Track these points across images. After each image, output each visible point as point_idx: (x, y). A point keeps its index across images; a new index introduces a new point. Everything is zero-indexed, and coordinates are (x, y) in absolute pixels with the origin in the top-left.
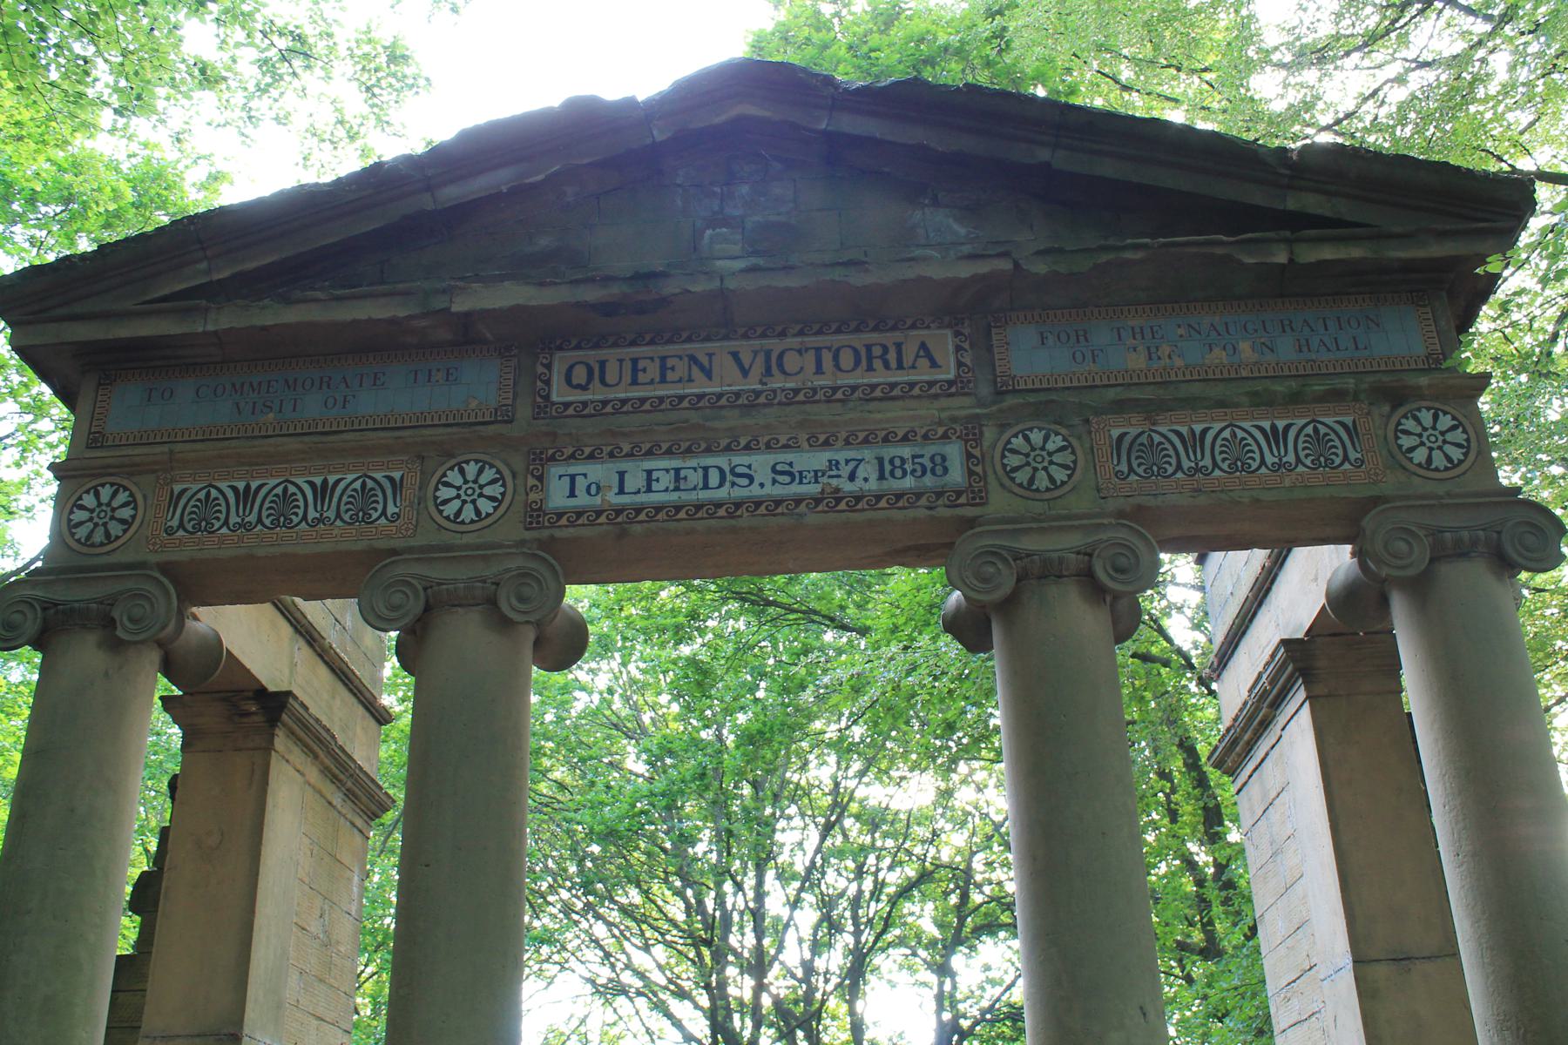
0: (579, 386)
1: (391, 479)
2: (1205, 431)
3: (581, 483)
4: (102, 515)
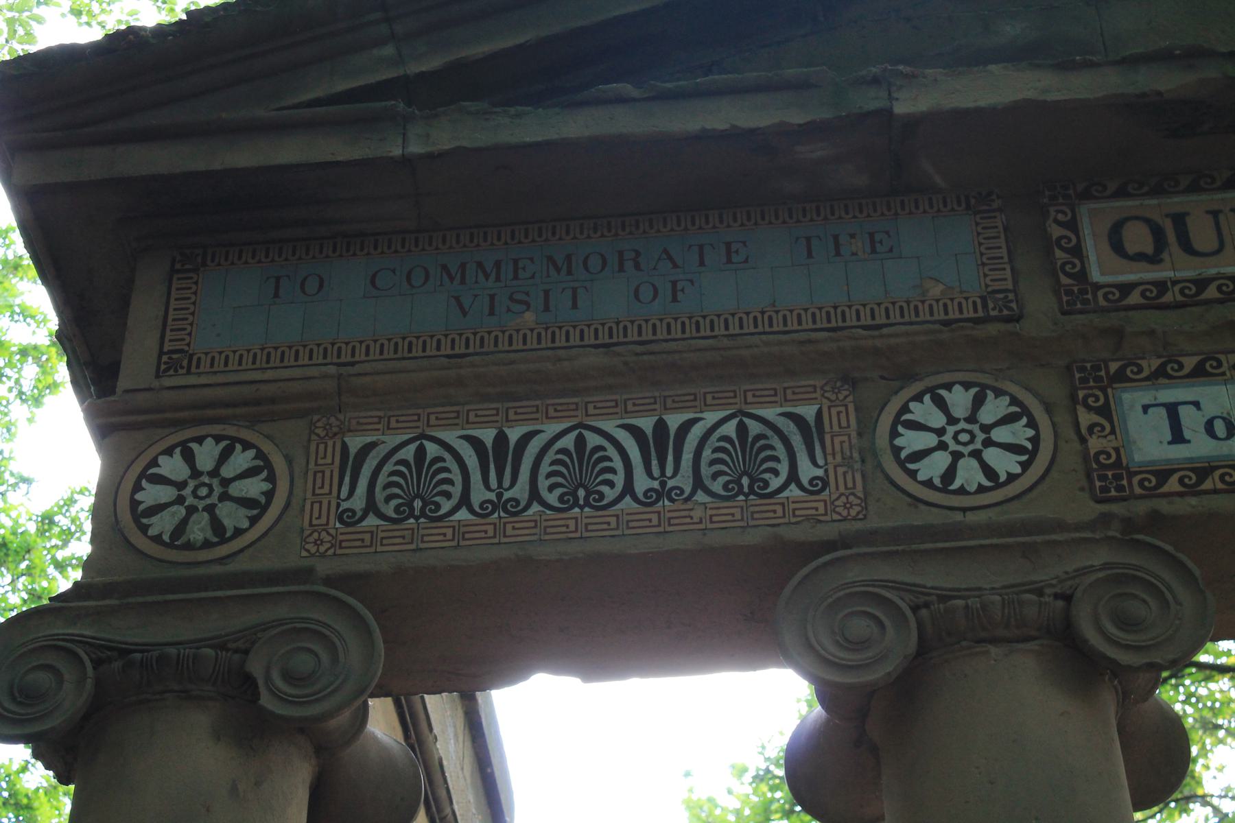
0: (1140, 257)
1: (798, 420)
2: (686, 427)
3: (1191, 420)
4: (203, 491)
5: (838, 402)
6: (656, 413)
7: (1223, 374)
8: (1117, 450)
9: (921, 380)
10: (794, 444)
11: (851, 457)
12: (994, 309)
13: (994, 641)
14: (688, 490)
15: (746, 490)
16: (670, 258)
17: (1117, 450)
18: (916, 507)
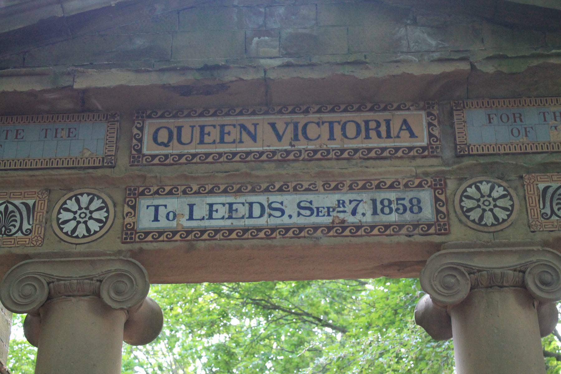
1: (26, 205)
3: (162, 212)
7: (178, 194)
8: (134, 223)
9: (73, 191)
10: (23, 215)
11: (42, 221)
12: (106, 163)
13: (73, 296)
17: (134, 223)
18: (60, 242)
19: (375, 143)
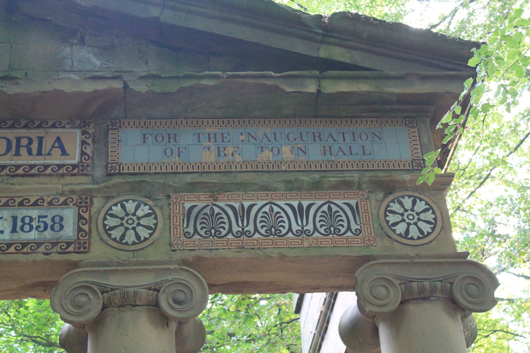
5: (363, 200)
6: (239, 201)
14: (252, 232)
15: (213, 234)
16: (332, 137)
19: (24, 160)
